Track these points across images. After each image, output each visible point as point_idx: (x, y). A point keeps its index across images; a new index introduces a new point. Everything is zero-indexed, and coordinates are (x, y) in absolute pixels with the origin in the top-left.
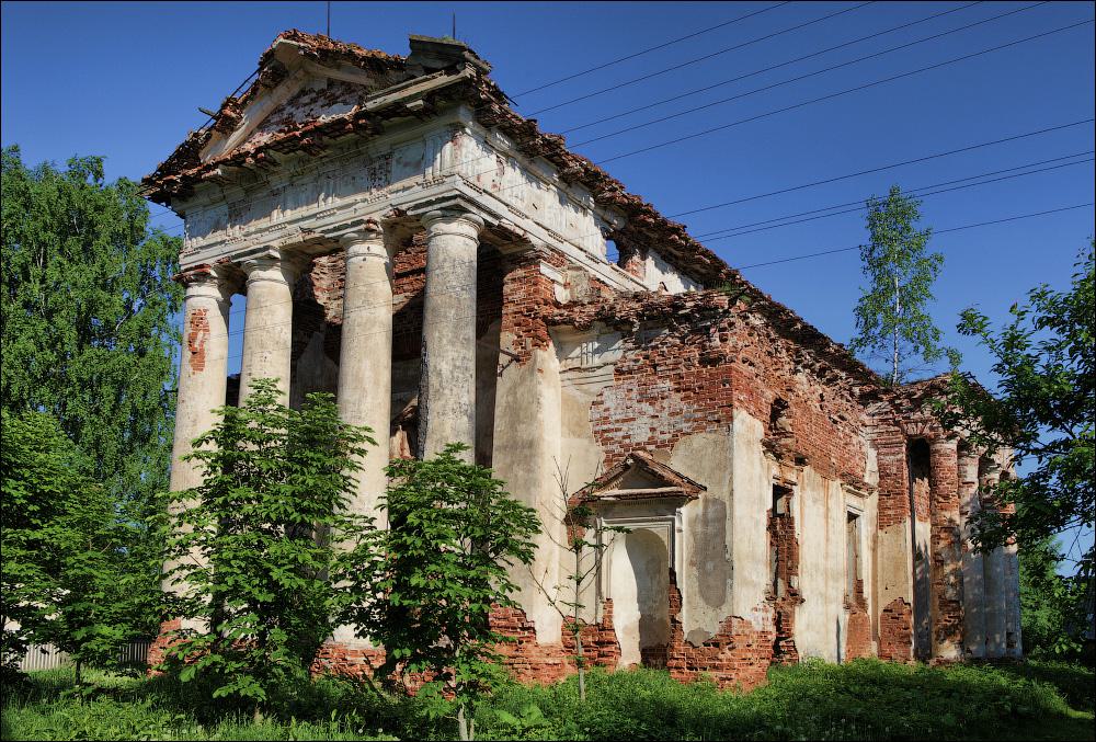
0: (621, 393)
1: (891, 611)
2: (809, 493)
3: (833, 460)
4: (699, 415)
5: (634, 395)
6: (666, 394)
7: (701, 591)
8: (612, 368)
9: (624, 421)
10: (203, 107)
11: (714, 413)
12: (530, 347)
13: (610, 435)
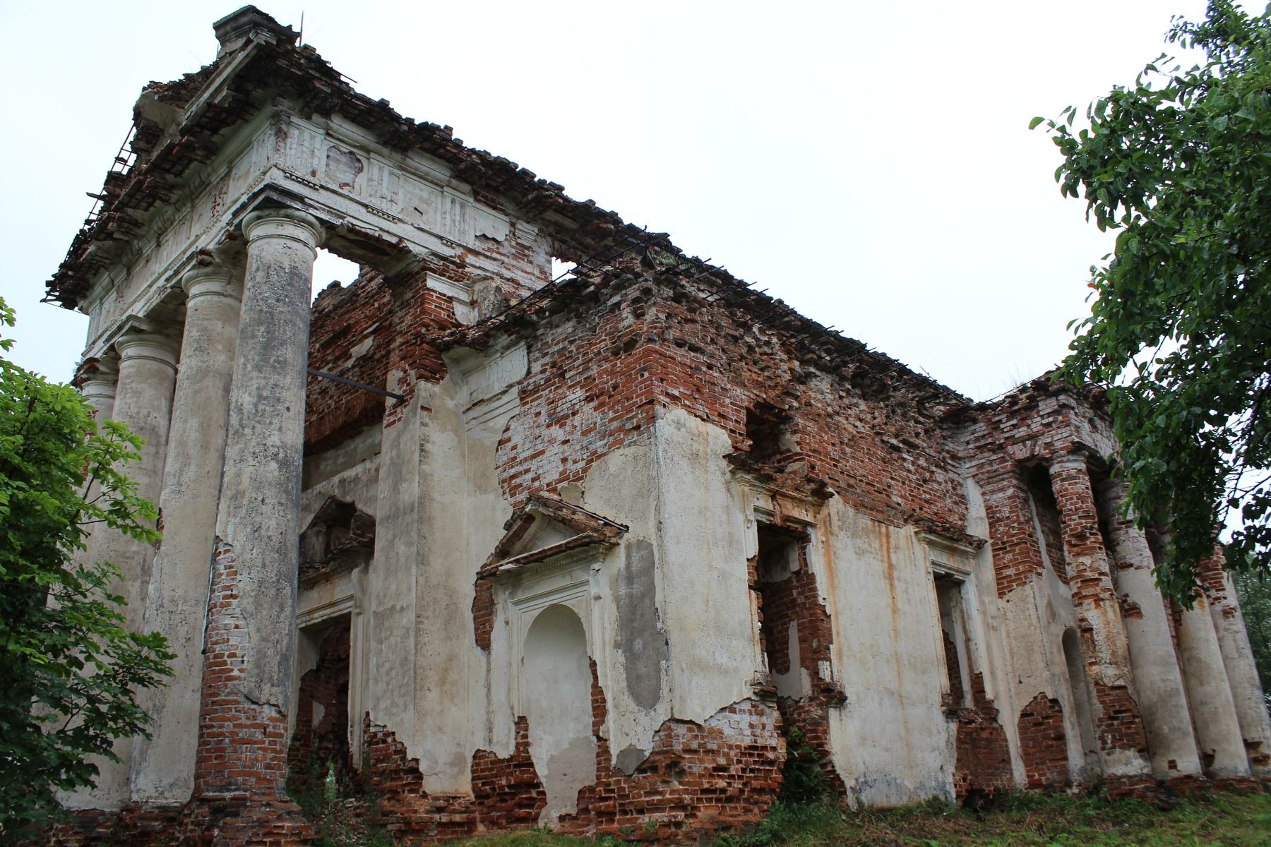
0: (529, 420)
1: (1032, 714)
2: (844, 545)
3: (896, 499)
4: (615, 424)
5: (543, 419)
6: (577, 407)
7: (629, 687)
8: (515, 391)
9: (534, 457)
10: (90, 192)
11: (632, 418)
12: (413, 381)
13: (518, 481)
